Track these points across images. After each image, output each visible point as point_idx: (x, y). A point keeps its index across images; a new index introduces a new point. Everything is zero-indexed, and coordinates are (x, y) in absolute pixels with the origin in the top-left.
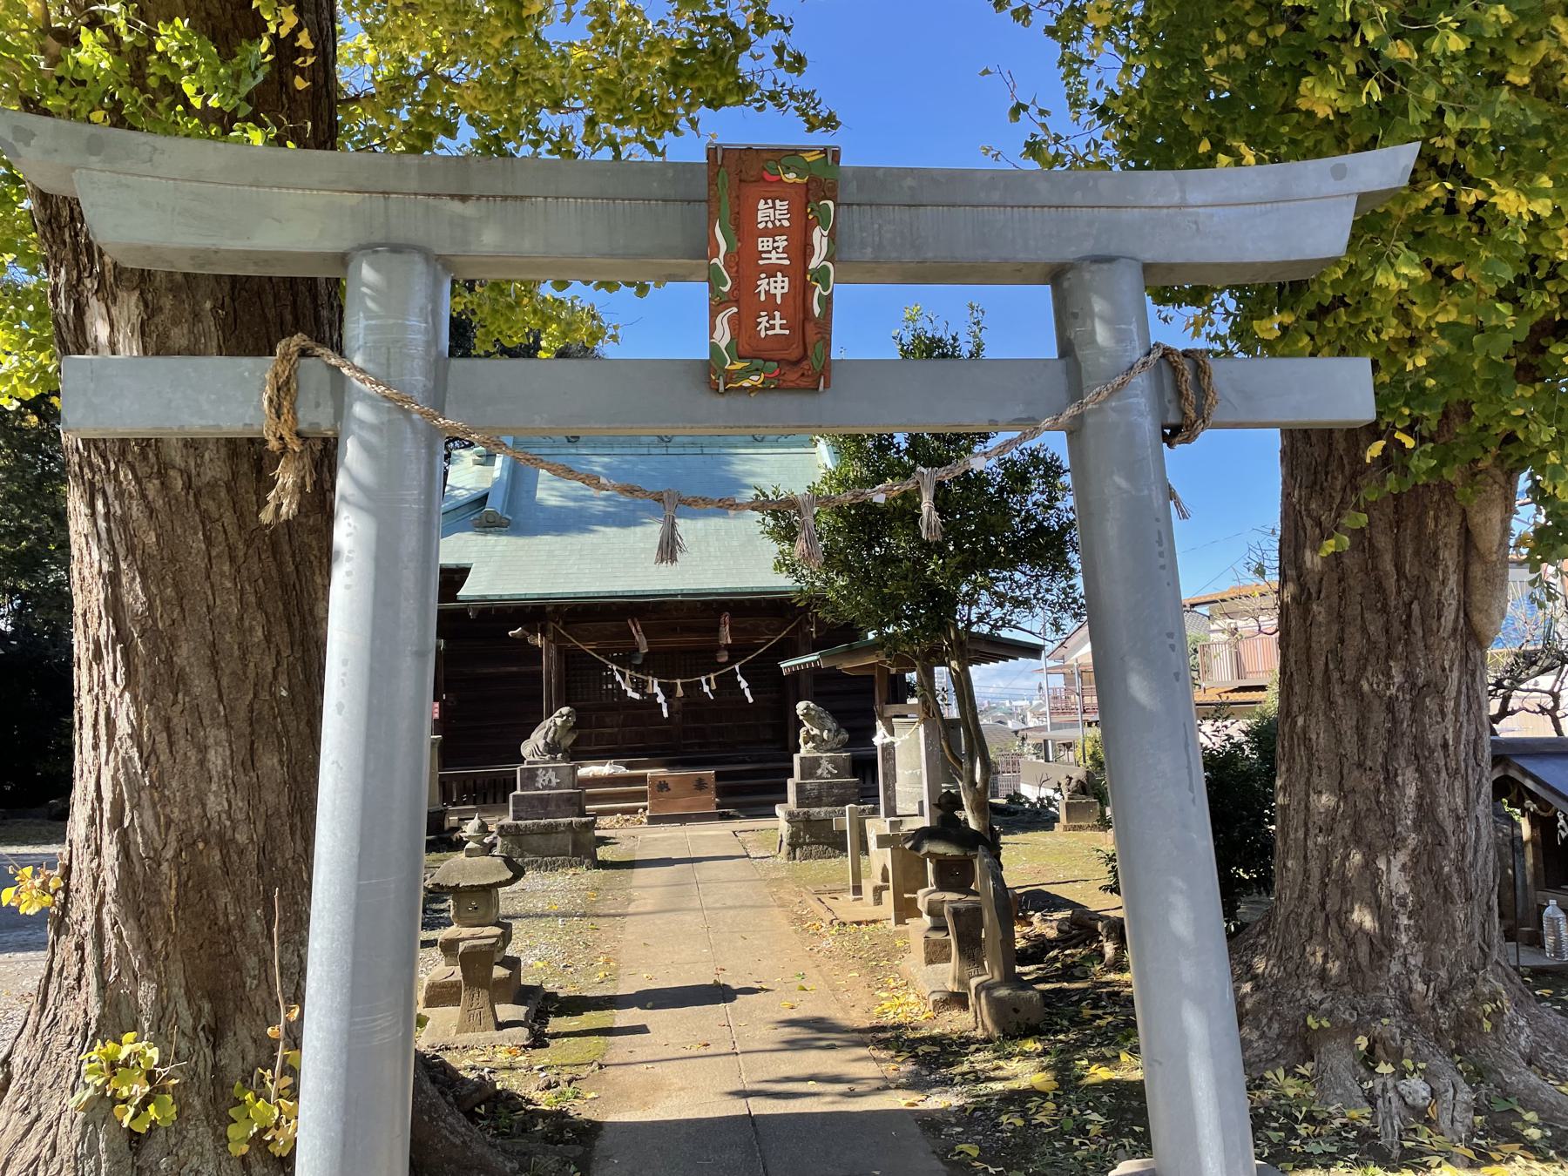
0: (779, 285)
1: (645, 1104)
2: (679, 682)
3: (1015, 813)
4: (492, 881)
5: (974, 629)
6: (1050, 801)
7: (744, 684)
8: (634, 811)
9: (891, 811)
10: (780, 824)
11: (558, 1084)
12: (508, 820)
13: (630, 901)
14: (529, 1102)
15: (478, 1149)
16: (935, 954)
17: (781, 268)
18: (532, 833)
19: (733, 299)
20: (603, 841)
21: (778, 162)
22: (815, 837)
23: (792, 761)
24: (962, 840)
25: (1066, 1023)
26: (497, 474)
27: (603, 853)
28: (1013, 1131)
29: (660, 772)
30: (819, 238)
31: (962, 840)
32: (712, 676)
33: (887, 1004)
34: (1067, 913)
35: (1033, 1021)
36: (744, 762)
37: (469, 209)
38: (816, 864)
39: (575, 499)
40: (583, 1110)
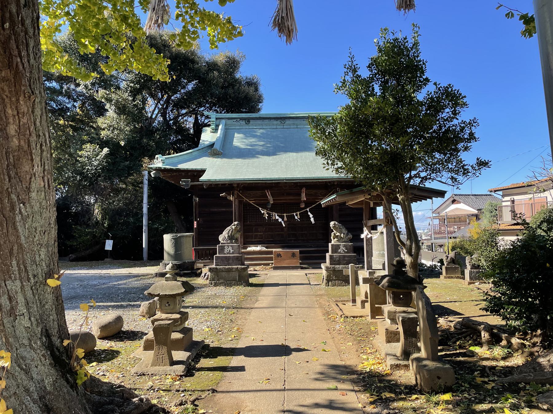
2: (285, 215)
4: (174, 293)
5: (412, 182)
7: (311, 216)
8: (268, 264)
9: (370, 267)
10: (323, 272)
12: (214, 266)
13: (257, 301)
18: (222, 271)
20: (254, 276)
22: (336, 278)
23: (328, 247)
24: (403, 283)
26: (218, 135)
27: (252, 280)
31: (403, 283)
32: (298, 213)
33: (366, 363)
34: (456, 319)
35: (449, 384)
36: (311, 247)
39: (251, 146)
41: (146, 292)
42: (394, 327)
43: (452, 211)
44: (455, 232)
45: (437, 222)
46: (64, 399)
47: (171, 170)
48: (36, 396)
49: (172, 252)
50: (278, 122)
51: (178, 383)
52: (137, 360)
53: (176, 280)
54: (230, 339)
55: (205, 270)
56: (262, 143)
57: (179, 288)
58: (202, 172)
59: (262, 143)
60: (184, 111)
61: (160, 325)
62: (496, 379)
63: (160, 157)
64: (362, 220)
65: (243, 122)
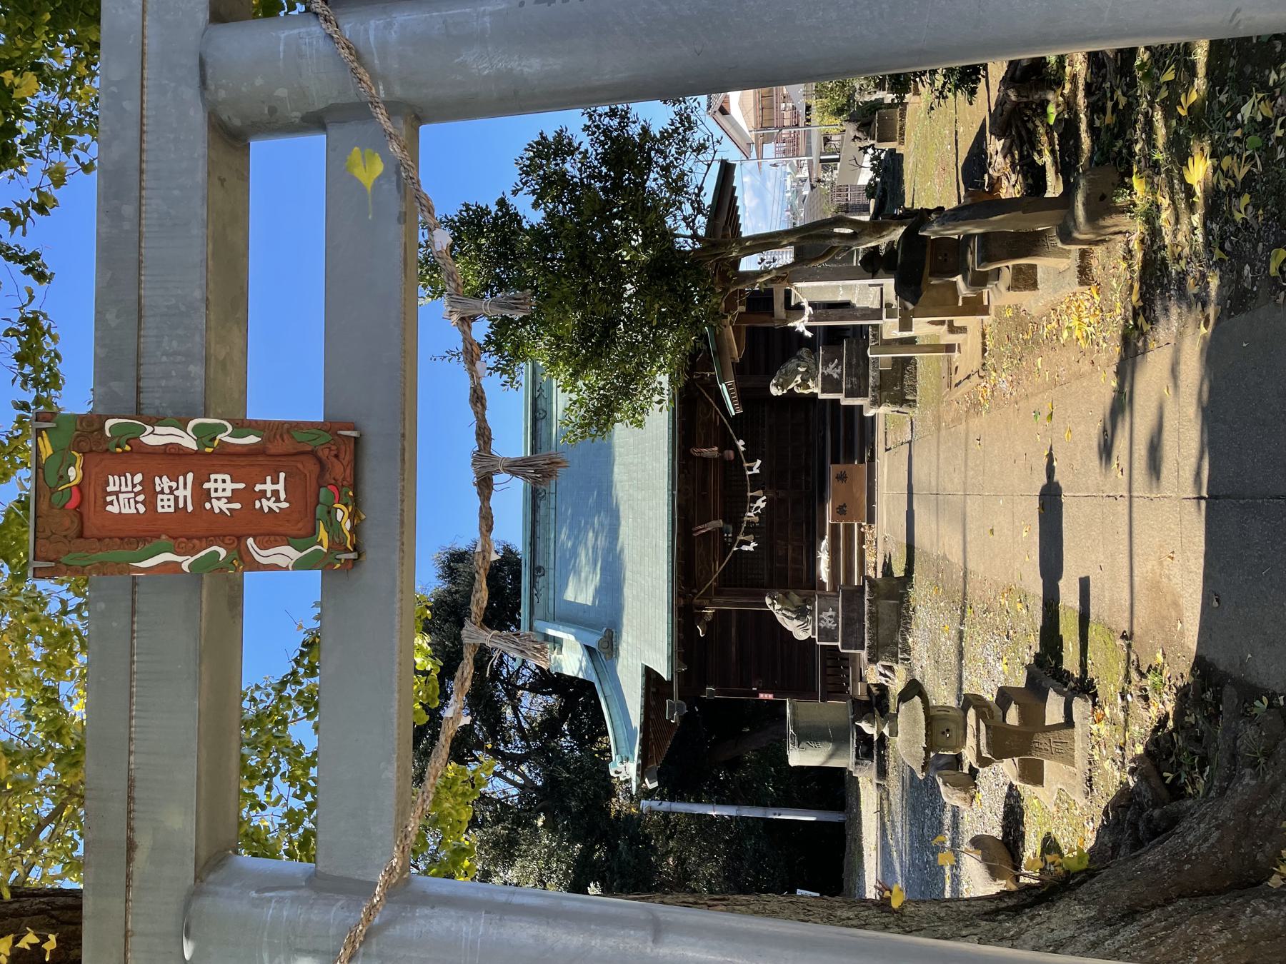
0: (220, 485)
1: (1176, 604)
2: (750, 494)
3: (884, 190)
4: (923, 717)
5: (701, 232)
6: (875, 158)
8: (862, 536)
9: (876, 314)
11: (1143, 689)
12: (864, 654)
14: (1162, 722)
15: (1225, 813)
16: (1025, 280)
17: (198, 483)
19: (235, 541)
20: (887, 568)
21: (53, 491)
22: (896, 384)
23: (825, 400)
25: (1120, 143)
26: (572, 638)
27: (898, 571)
28: (1256, 207)
29: (829, 508)
30: (156, 437)
33: (1077, 333)
34: (995, 145)
37: (144, 841)
38: (921, 383)
40: (1180, 669)
41: (921, 776)
42: (1007, 276)
43: (745, 115)
44: (794, 108)
45: (769, 149)
46: (1113, 887)
47: (644, 743)
48: (1107, 932)
49: (829, 748)
50: (542, 504)
51: (1107, 711)
52: (1062, 800)
53: (896, 715)
54: (1024, 611)
55: (873, 675)
56: (591, 534)
57: (914, 708)
58: (649, 674)
59: (591, 534)
60: (509, 713)
61: (988, 743)
62: (1108, 85)
63: (615, 765)
64: (773, 328)
65: (541, 580)
